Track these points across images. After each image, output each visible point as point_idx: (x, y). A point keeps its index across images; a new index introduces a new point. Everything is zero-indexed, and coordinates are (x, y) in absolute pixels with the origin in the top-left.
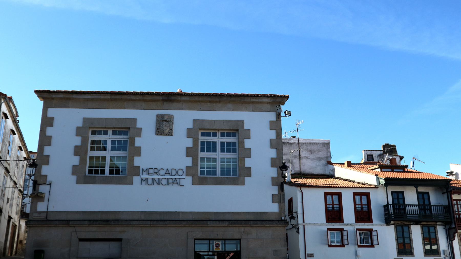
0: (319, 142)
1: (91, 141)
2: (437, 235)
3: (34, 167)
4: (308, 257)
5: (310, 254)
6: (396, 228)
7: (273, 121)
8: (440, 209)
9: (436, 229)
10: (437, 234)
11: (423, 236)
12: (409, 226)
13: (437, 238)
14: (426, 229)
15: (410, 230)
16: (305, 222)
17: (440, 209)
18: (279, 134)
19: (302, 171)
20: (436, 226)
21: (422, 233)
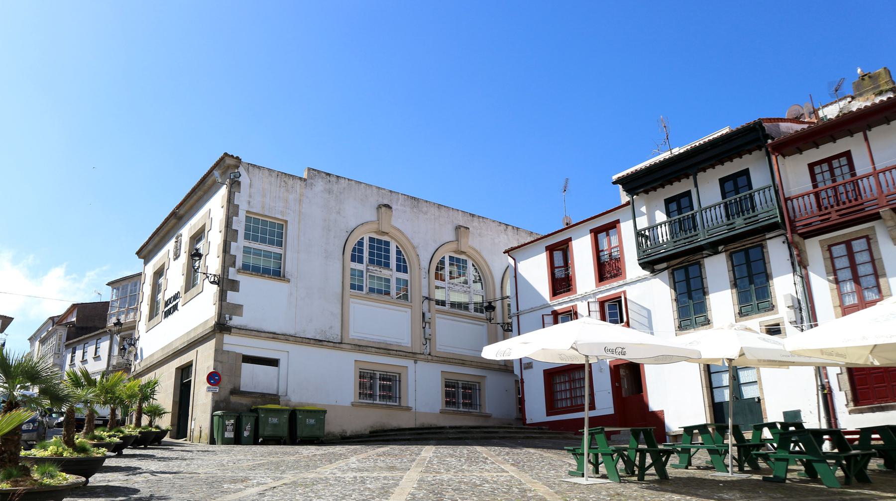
0: (631, 171)
1: (242, 314)
2: (767, 265)
3: (491, 311)
4: (525, 368)
5: (527, 363)
6: (672, 276)
7: (232, 290)
8: (870, 186)
9: (764, 250)
10: (766, 261)
11: (732, 276)
12: (700, 261)
13: (768, 272)
14: (740, 258)
15: (702, 270)
16: (519, 310)
17: (870, 186)
18: (222, 296)
19: (835, 170)
20: (764, 243)
21: (731, 269)
